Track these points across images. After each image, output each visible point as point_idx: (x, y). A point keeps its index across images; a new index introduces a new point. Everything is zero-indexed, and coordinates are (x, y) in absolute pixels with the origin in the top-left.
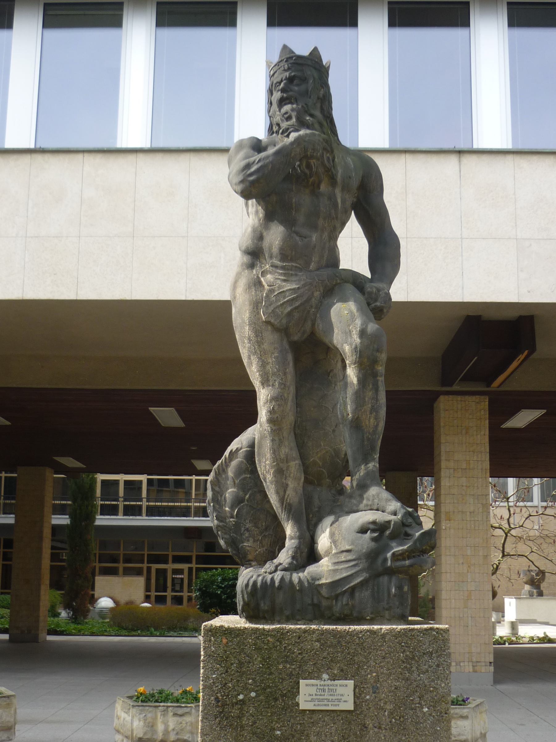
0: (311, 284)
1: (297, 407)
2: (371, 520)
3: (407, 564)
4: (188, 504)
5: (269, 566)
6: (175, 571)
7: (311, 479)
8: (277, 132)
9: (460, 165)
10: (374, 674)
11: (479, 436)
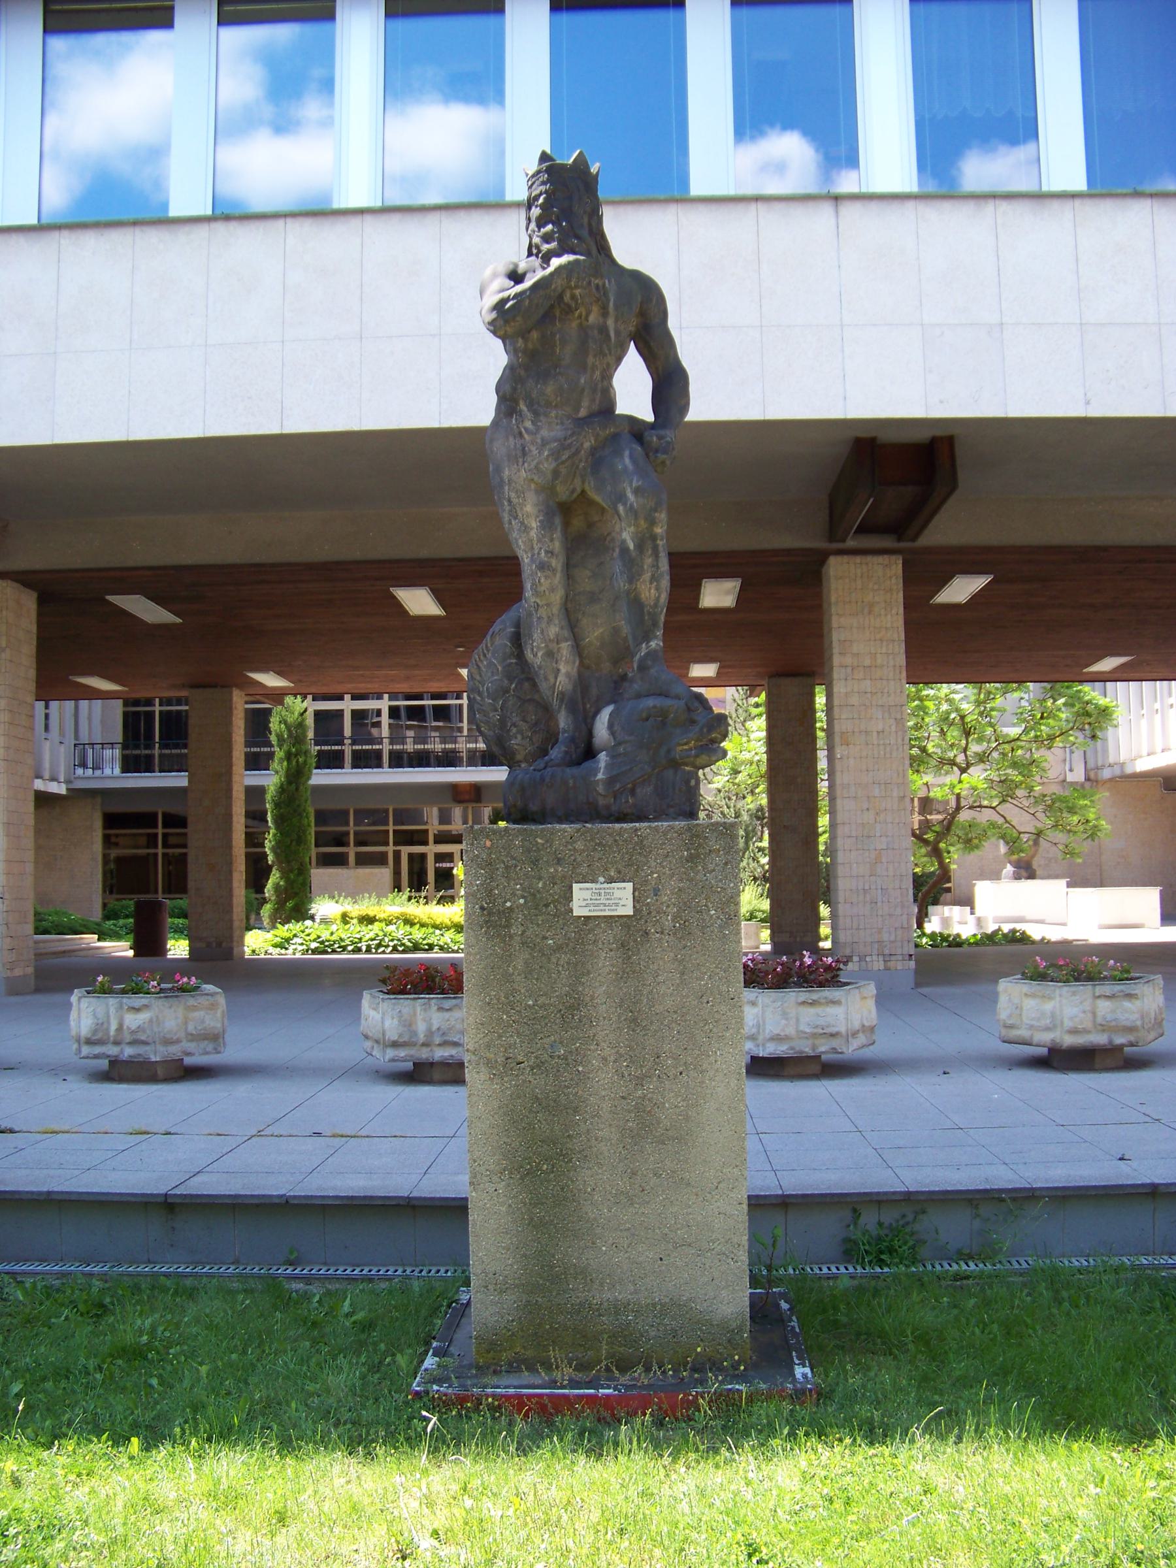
6: (440, 857)
8: (537, 256)
9: (837, 217)
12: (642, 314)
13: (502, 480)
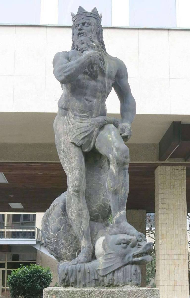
0: (93, 124)
1: (86, 183)
2: (122, 238)
3: (140, 260)
4: (3, 230)
5: (75, 261)
7: (94, 218)
11: (181, 190)
13: (60, 142)
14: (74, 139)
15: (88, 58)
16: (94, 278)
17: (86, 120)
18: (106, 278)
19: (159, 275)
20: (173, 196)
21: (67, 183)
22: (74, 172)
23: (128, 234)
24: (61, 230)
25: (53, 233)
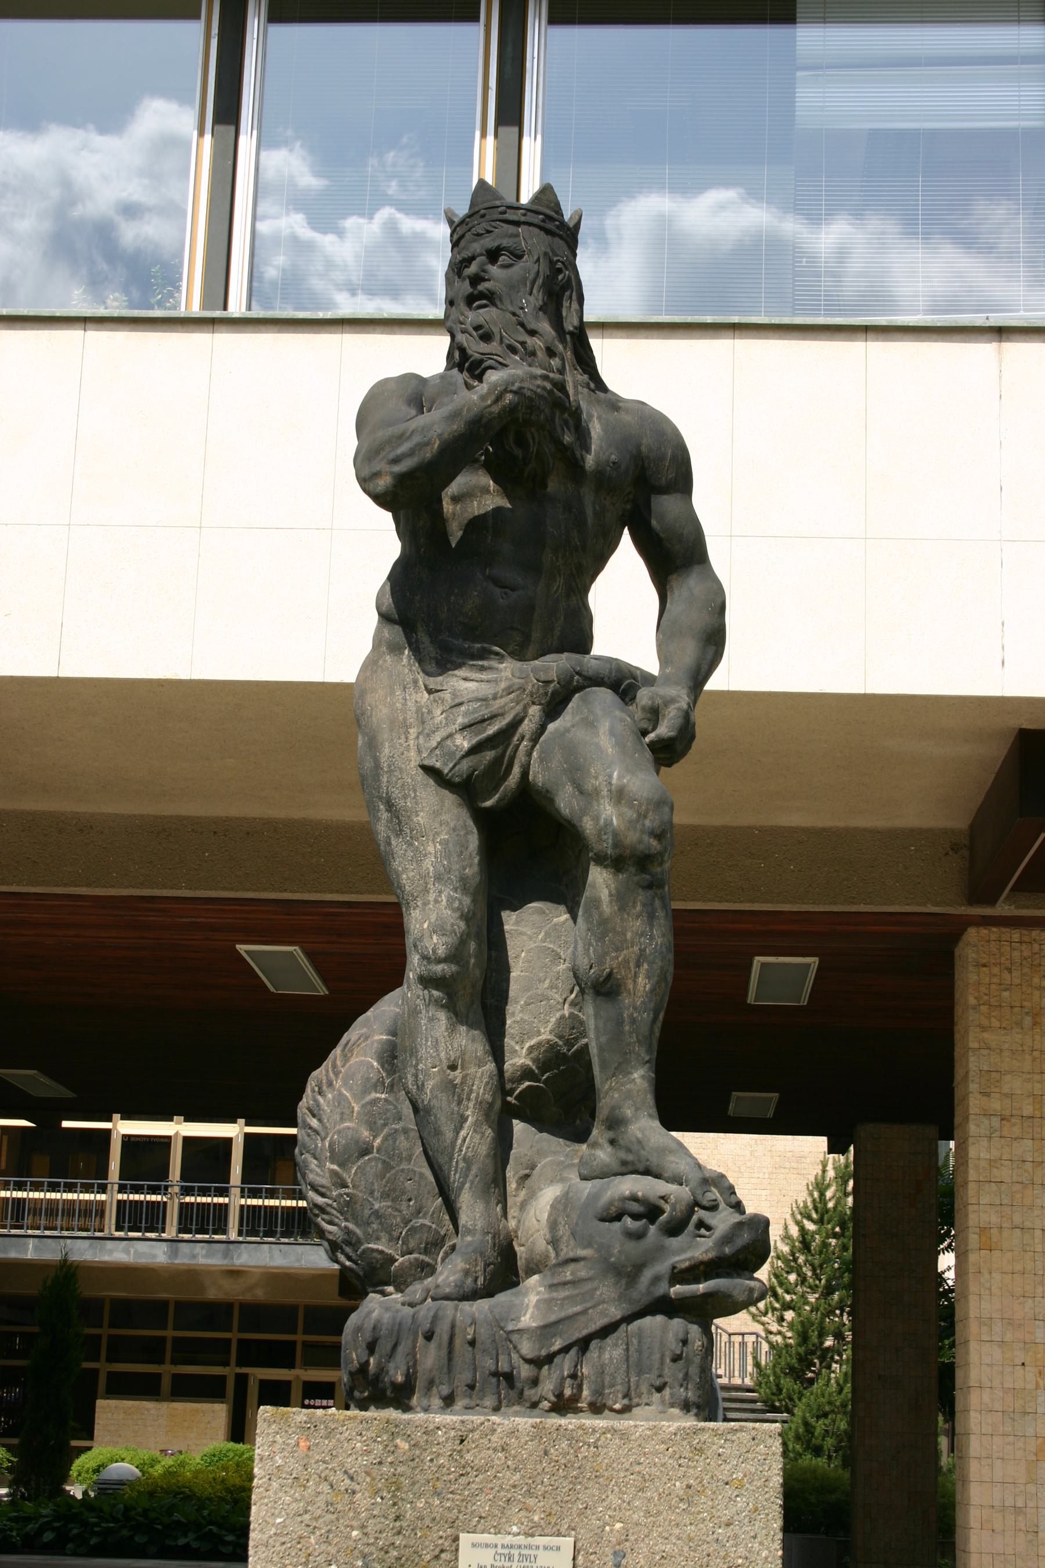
9: (1000, 361)
10: (618, 1526)
12: (645, 490)
14: (437, 752)
15: (499, 398)
16: (493, 1368)
17: (490, 668)
18: (549, 1369)
19: (967, 1411)
20: (1034, 1060)
21: (404, 945)
22: (432, 897)
23: (658, 1176)
24: (375, 1154)
25: (339, 1165)
